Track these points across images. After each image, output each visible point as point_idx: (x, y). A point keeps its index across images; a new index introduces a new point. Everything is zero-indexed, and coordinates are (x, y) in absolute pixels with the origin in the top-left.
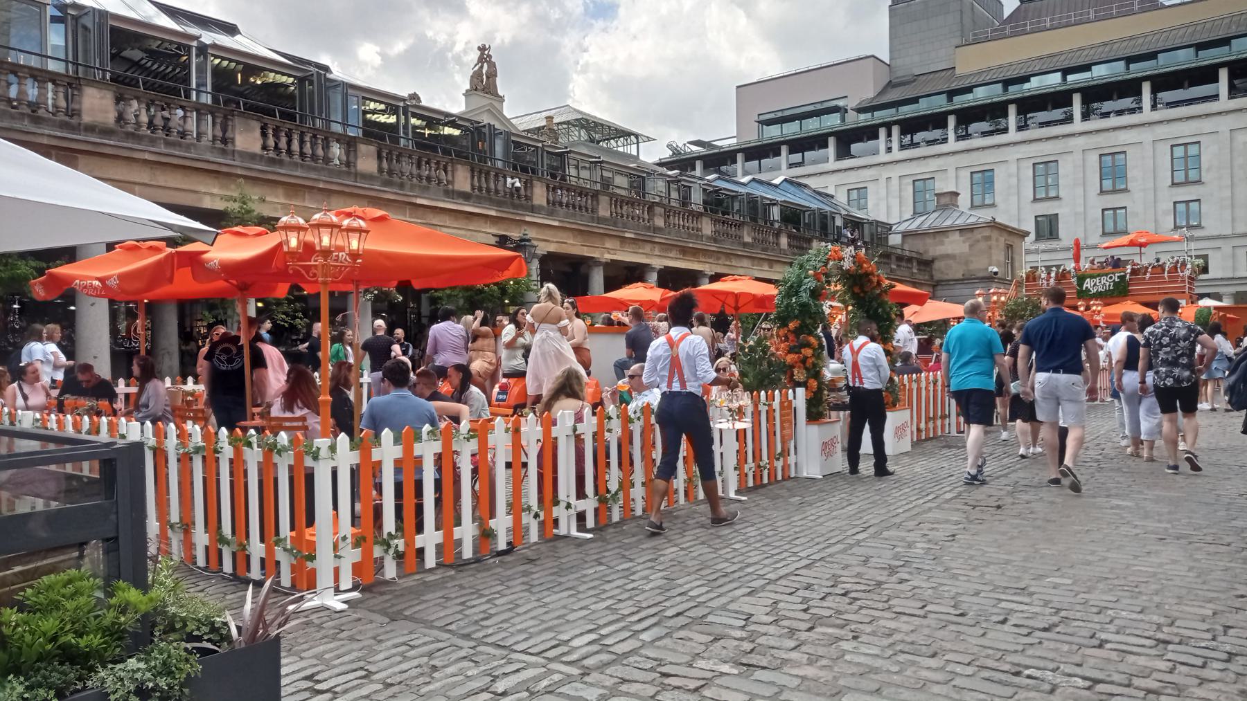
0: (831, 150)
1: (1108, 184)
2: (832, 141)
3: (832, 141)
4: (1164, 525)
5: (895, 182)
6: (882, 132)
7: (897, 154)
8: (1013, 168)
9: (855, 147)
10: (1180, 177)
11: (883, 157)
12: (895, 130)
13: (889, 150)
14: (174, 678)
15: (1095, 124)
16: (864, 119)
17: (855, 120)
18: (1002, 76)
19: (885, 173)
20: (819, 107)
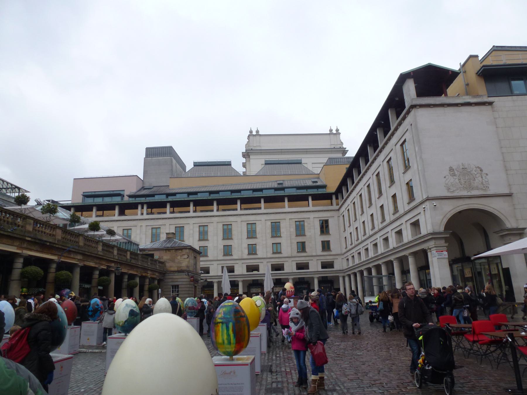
0: (117, 211)
6: (140, 207)
8: (191, 227)
9: (127, 211)
11: (139, 217)
12: (145, 207)
13: (142, 214)
16: (132, 200)
17: (126, 199)
19: (140, 223)
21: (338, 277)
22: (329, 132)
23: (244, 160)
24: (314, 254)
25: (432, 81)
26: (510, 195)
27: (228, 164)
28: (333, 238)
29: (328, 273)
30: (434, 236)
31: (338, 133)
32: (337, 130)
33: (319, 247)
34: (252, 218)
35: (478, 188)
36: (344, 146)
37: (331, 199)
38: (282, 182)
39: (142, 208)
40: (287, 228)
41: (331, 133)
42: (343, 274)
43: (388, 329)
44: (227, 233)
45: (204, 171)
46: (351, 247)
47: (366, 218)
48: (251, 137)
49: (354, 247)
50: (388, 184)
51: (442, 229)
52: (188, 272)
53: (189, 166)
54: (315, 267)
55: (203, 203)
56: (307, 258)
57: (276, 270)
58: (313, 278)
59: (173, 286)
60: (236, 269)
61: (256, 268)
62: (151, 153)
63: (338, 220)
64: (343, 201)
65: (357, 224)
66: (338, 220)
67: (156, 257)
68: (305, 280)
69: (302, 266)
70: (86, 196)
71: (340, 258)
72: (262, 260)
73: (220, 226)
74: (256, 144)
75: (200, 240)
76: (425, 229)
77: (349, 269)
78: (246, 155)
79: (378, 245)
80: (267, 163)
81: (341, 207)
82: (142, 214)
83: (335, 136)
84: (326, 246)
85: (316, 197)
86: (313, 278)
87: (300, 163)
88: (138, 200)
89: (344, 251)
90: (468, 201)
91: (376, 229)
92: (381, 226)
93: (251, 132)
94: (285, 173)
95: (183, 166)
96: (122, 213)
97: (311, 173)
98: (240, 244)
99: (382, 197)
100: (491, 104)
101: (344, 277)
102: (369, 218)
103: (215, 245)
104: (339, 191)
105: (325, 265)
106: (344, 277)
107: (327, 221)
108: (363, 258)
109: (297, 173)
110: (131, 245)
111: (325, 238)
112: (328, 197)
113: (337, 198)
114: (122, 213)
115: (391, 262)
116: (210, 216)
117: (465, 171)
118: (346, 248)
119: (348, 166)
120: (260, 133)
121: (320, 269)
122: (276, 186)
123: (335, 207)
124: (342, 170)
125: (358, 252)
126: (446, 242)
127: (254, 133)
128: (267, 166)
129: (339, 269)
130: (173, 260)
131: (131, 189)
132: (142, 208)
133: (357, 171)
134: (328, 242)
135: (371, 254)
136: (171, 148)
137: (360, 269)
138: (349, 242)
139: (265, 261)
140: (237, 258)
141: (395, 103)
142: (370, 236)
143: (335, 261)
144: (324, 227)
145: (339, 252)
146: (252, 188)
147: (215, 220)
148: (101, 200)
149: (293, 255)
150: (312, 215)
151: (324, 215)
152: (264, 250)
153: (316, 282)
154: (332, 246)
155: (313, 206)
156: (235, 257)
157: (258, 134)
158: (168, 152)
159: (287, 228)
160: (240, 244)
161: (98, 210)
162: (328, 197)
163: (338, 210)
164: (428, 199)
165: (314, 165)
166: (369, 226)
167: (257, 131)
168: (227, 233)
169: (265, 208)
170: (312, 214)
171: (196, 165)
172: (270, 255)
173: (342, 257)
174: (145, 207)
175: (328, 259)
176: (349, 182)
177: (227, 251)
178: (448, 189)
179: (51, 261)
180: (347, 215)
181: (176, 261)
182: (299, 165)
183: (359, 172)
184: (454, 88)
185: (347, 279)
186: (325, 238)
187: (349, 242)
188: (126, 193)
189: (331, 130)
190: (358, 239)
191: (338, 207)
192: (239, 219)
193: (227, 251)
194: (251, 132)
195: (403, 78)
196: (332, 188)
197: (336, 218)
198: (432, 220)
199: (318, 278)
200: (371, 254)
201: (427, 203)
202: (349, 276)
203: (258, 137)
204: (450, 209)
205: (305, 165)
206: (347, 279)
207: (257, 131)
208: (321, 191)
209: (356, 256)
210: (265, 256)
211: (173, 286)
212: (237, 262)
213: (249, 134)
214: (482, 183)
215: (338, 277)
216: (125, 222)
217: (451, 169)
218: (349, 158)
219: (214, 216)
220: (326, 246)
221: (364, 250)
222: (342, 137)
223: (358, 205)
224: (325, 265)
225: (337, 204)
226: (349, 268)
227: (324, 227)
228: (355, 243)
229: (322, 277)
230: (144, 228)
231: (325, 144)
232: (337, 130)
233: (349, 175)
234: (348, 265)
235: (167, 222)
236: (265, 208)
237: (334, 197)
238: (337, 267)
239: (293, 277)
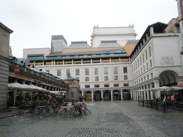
0: (43, 63)
1: (88, 70)
2: (43, 62)
3: (43, 62)
4: (181, 133)
5: (54, 70)
6: (52, 61)
7: (55, 65)
8: (73, 70)
9: (46, 63)
10: (97, 69)
11: (52, 65)
12: (54, 61)
13: (53, 64)
14: (178, 126)
15: (45, 66)
16: (48, 58)
17: (45, 58)
18: (71, 54)
19: (53, 68)
20: (39, 55)
21: (130, 89)
22: (129, 26)
23: (91, 38)
24: (121, 81)
25: (159, 28)
26: (181, 66)
27: (86, 42)
28: (128, 74)
29: (126, 88)
30: (156, 79)
31: (133, 26)
32: (133, 25)
33: (123, 78)
34: (97, 67)
35: (170, 64)
36: (136, 32)
37: (128, 58)
39: (53, 62)
41: (130, 27)
42: (132, 89)
44: (87, 72)
45: (76, 46)
46: (135, 78)
47: (145, 64)
48: (95, 29)
49: (138, 78)
50: (149, 56)
51: (158, 77)
52: (77, 88)
53: (69, 44)
55: (77, 60)
56: (118, 82)
57: (106, 86)
58: (120, 90)
59: (71, 93)
60: (90, 86)
61: (88, 86)
62: (54, 38)
63: (131, 67)
64: (143, 46)
65: (144, 64)
66: (131, 67)
67: (65, 82)
68: (118, 90)
69: (107, 86)
70: (29, 56)
71: (131, 82)
72: (101, 83)
73: (84, 69)
74: (97, 32)
75: (76, 75)
76: (154, 76)
77: (134, 86)
78: (93, 37)
79: (149, 76)
80: (102, 42)
81: (132, 62)
82: (53, 64)
83: (132, 28)
84: (126, 77)
85: (122, 58)
86: (120, 90)
87: (115, 42)
88: (51, 58)
89: (133, 79)
90: (167, 68)
91: (149, 69)
92: (150, 68)
93: (95, 26)
94: (110, 47)
95: (66, 42)
96: (45, 64)
98: (92, 77)
99: (151, 57)
100: (178, 36)
101: (132, 90)
102: (150, 62)
103: (82, 77)
104: (131, 56)
106: (132, 90)
107: (126, 68)
108: (144, 81)
109: (114, 47)
111: (125, 74)
112: (127, 57)
113: (130, 58)
114: (45, 64)
115: (136, 88)
116: (80, 66)
117: (167, 58)
118: (133, 78)
119: (136, 44)
120: (99, 27)
121: (123, 86)
123: (129, 62)
124: (133, 47)
125: (151, 73)
126: (159, 80)
127: (96, 27)
131: (47, 53)
132: (53, 62)
133: (142, 44)
135: (147, 79)
136: (62, 36)
137: (145, 84)
138: (143, 71)
139: (102, 83)
140: (91, 82)
141: (148, 31)
142: (141, 76)
143: (129, 83)
144: (125, 70)
146: (96, 53)
147: (82, 67)
148: (35, 58)
150: (120, 65)
151: (125, 65)
152: (102, 79)
153: (121, 91)
154: (128, 77)
155: (121, 61)
156: (90, 82)
157: (98, 27)
158: (61, 37)
160: (92, 77)
161: (35, 62)
162: (127, 57)
163: (131, 63)
164: (154, 67)
165: (122, 43)
166: (146, 67)
167: (97, 26)
168: (87, 72)
169: (102, 62)
170: (120, 65)
171: (73, 43)
172: (104, 81)
173: (132, 82)
174: (54, 61)
175: (126, 82)
176: (141, 45)
177: (87, 79)
178: (161, 64)
179: (49, 86)
180: (142, 57)
183: (146, 41)
184: (167, 29)
185: (133, 90)
187: (143, 71)
188: (45, 55)
189: (130, 25)
190: (148, 69)
191: (131, 62)
192: (91, 67)
193: (87, 79)
194: (95, 26)
195: (149, 27)
196: (129, 54)
197: (130, 66)
198: (156, 74)
199: (122, 90)
200: (147, 79)
201: (154, 68)
202: (134, 89)
203: (98, 29)
204: (161, 70)
205: (118, 43)
206: (133, 90)
207: (97, 26)
208: (125, 55)
209: (141, 80)
211: (71, 93)
212: (91, 83)
213: (94, 27)
214: (172, 62)
215: (130, 89)
216: (47, 68)
217: (163, 58)
218: (136, 40)
220: (126, 77)
221: (150, 74)
222: (135, 28)
223: (142, 59)
226: (146, 81)
227: (125, 70)
228: (146, 70)
229: (124, 89)
231: (127, 31)
232: (133, 25)
233: (136, 48)
234: (136, 84)
236: (102, 62)
237: (129, 58)
238: (130, 86)
239: (113, 89)
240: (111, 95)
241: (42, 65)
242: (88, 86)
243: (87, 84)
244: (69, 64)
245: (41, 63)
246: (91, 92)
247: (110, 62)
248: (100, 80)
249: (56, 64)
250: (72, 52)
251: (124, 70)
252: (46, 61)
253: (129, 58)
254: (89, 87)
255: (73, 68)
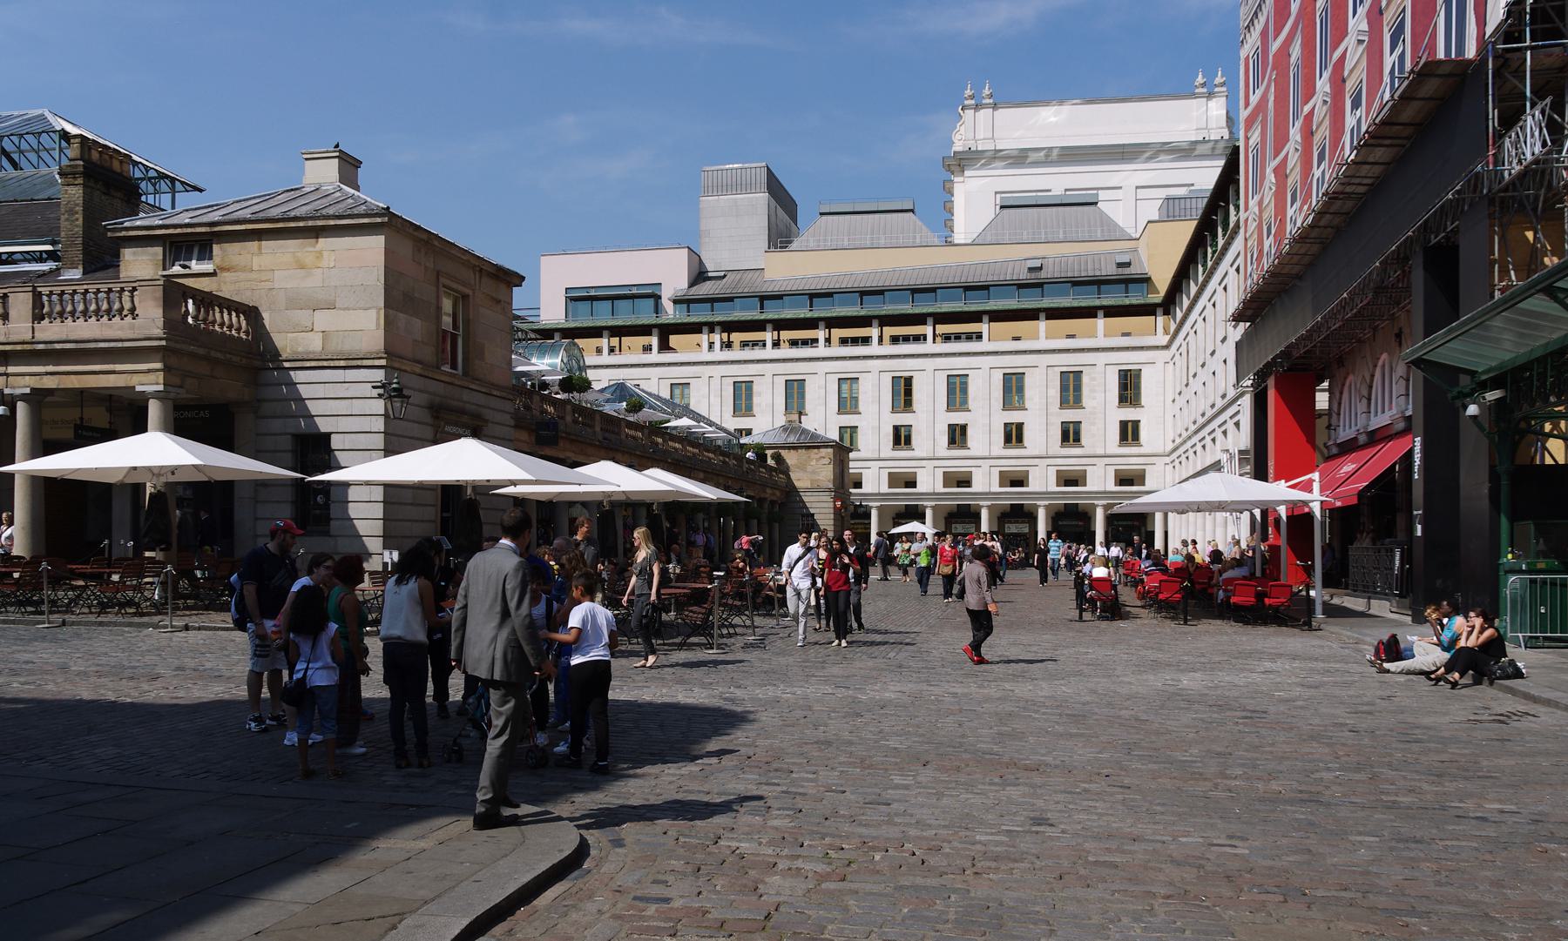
0: (654, 341)
2: (655, 331)
5: (715, 382)
7: (719, 355)
9: (674, 340)
11: (706, 356)
13: (711, 345)
17: (671, 313)
24: (1101, 452)
28: (1147, 415)
38: (1037, 264)
40: (1041, 389)
43: (811, 476)
54: (1100, 480)
57: (1068, 483)
61: (1018, 481)
69: (1071, 479)
82: (711, 345)
84: (1129, 432)
96: (665, 346)
97: (1118, 235)
103: (874, 424)
105: (1125, 479)
107: (908, 381)
110: (173, 192)
111: (1129, 414)
122: (1024, 275)
128: (1006, 211)
129: (1095, 489)
130: (802, 467)
134: (1136, 424)
140: (924, 455)
144: (1129, 388)
145: (1160, 450)
149: (1050, 453)
156: (917, 453)
159: (1041, 389)
162: (1147, 310)
181: (809, 469)
182: (1092, 208)
186: (1129, 414)
188: (666, 295)
191: (1164, 340)
197: (1160, 365)
210: (986, 454)
212: (924, 463)
219: (871, 357)
220: (1129, 432)
224: (1125, 479)
225: (1166, 332)
227: (1129, 388)
230: (715, 382)
235: (768, 367)
240: (1153, 533)
241: (647, 349)
242: (964, 481)
243: (903, 467)
244: (855, 341)
245: (643, 340)
246: (977, 517)
247: (1042, 334)
248: (921, 444)
249: (728, 345)
250: (823, 271)
251: (1064, 388)
252: (666, 332)
253: (1160, 311)
254: (913, 484)
255: (822, 367)
